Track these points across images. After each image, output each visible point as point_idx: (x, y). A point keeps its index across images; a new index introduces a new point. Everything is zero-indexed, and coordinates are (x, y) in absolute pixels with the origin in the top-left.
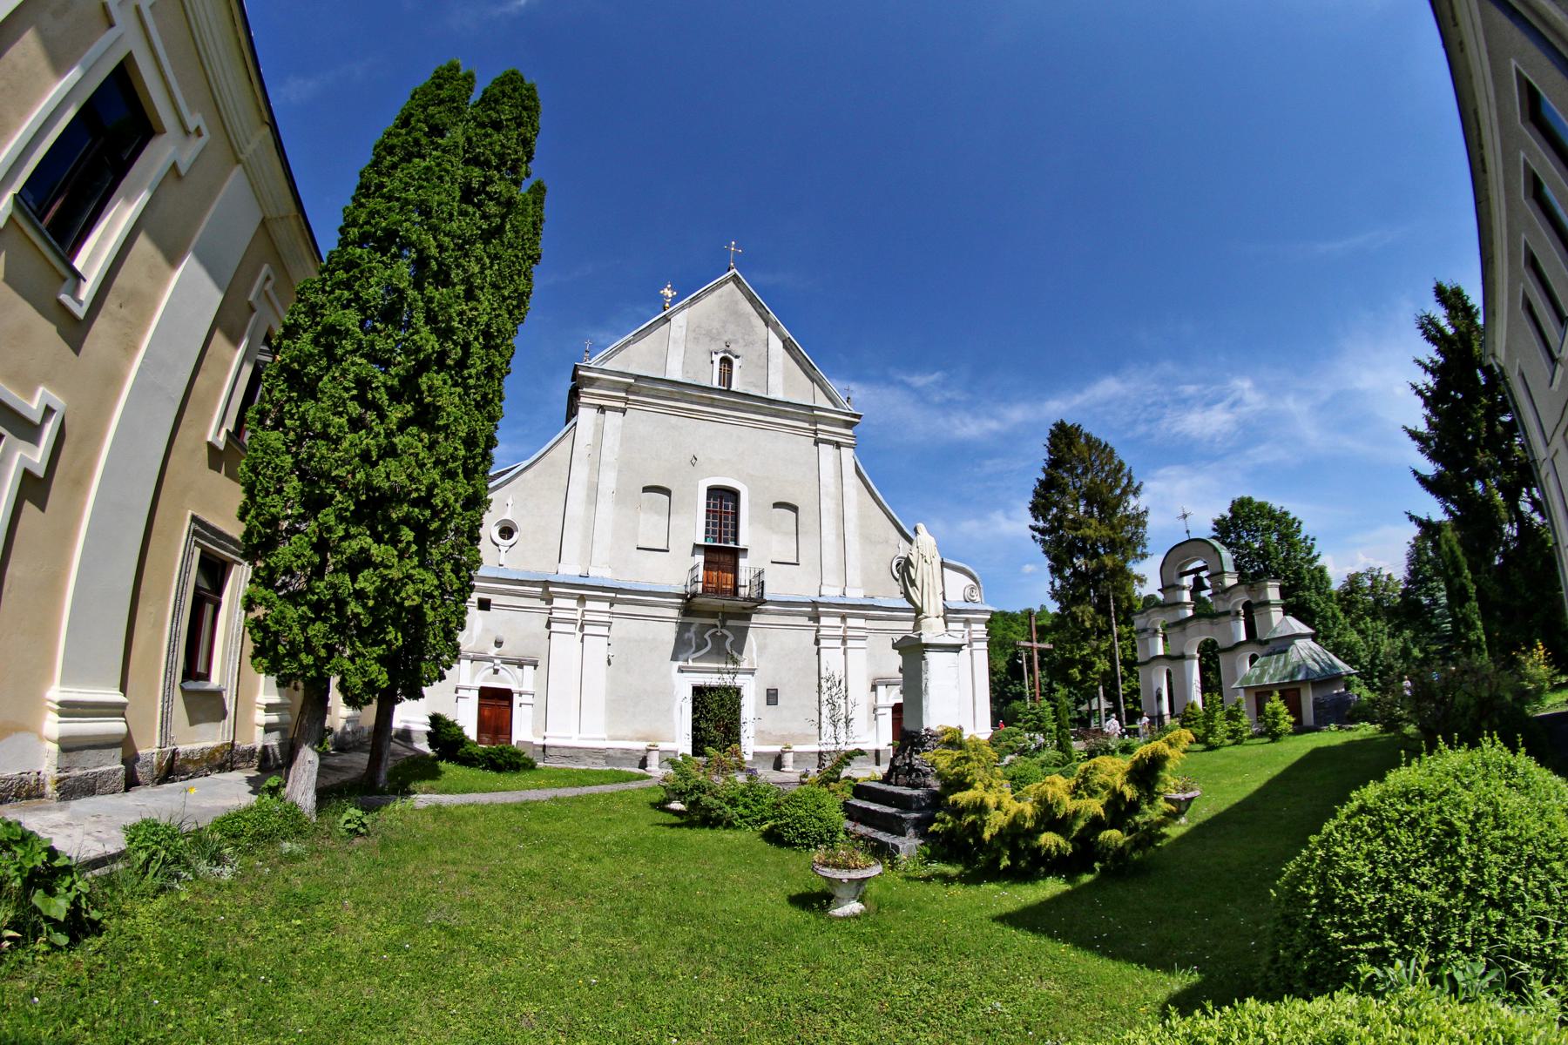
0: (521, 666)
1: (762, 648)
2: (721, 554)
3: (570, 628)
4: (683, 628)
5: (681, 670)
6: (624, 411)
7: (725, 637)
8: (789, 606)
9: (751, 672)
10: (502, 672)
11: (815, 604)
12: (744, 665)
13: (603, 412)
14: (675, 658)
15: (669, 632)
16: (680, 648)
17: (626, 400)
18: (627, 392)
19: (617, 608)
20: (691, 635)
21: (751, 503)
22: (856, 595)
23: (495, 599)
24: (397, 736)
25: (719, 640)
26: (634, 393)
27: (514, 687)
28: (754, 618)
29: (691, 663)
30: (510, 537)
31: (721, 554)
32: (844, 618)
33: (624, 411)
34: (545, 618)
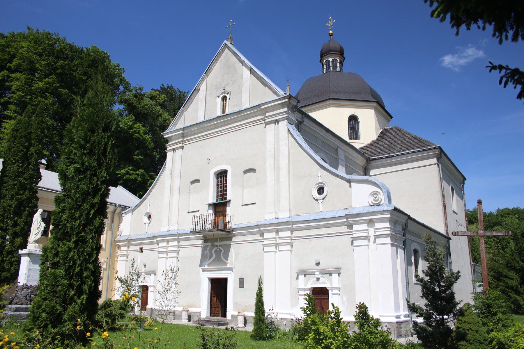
0: (331, 274)
1: (237, 255)
2: (220, 207)
3: (365, 242)
4: (204, 248)
5: (203, 271)
6: (182, 148)
7: (221, 251)
8: (247, 229)
9: (231, 269)
10: (146, 278)
11: (347, 217)
12: (229, 265)
13: (278, 122)
14: (201, 265)
15: (198, 252)
16: (204, 258)
17: (182, 142)
18: (183, 137)
19: (296, 234)
20: (207, 252)
21: (232, 174)
22: (284, 216)
23: (145, 247)
24: (102, 308)
25: (218, 253)
26: (187, 136)
27: (328, 286)
28: (234, 239)
29: (206, 267)
30: (323, 192)
31: (220, 207)
32: (277, 232)
33: (182, 148)
34: (348, 239)
